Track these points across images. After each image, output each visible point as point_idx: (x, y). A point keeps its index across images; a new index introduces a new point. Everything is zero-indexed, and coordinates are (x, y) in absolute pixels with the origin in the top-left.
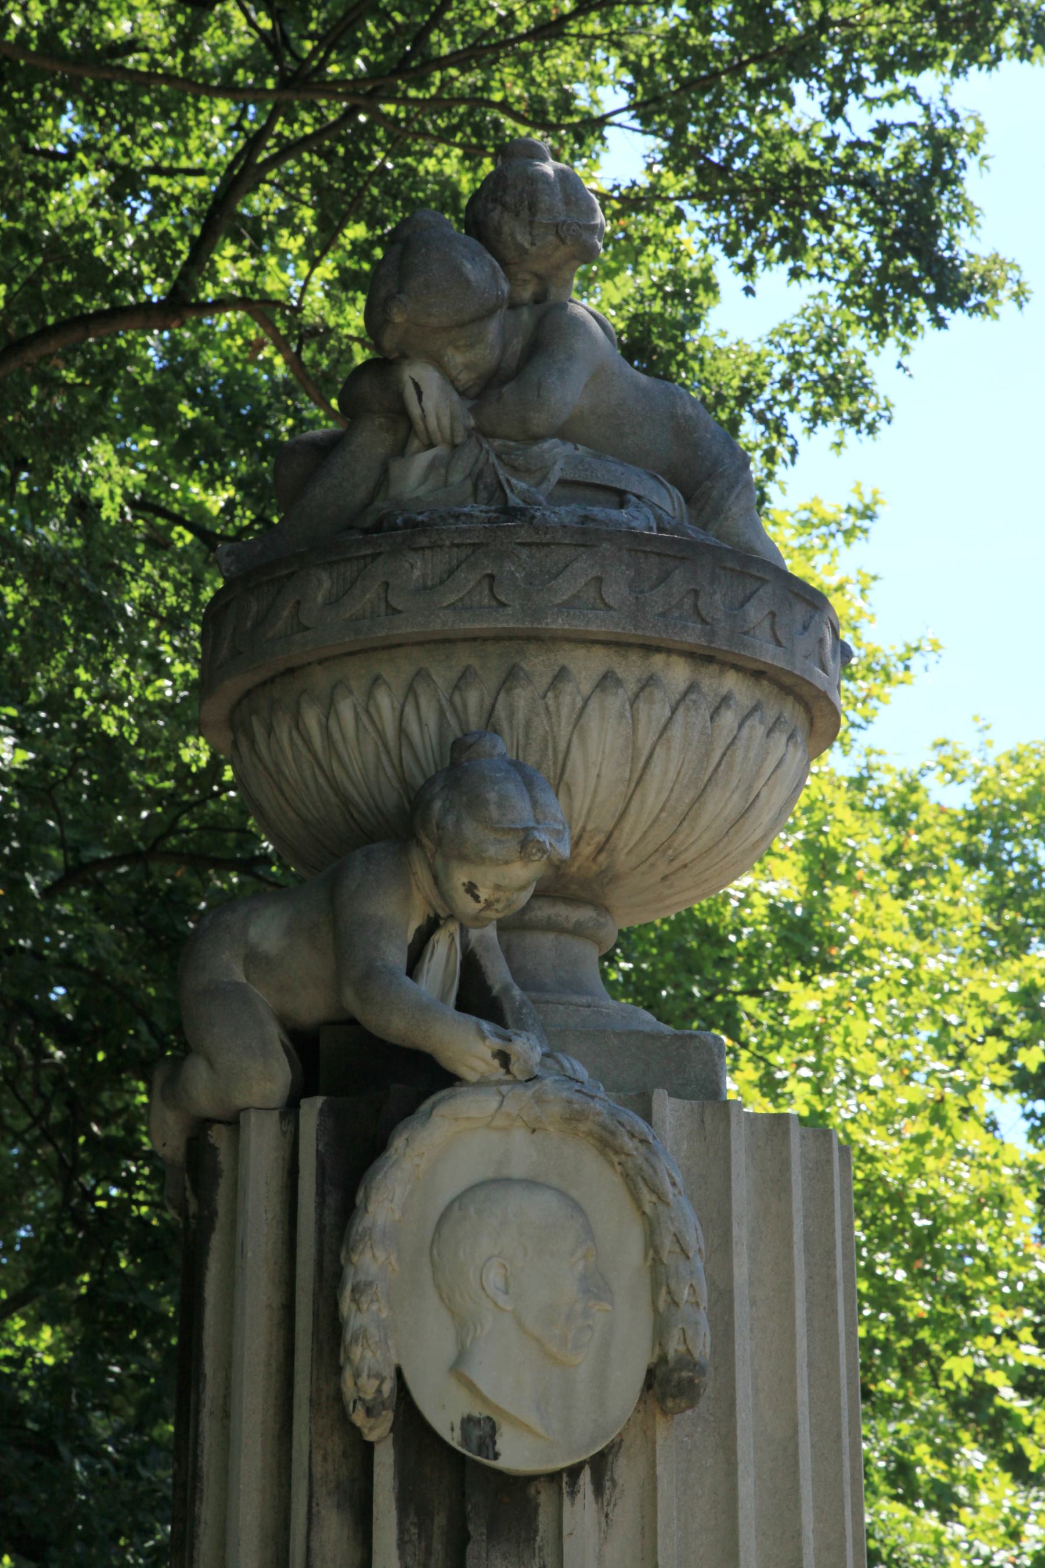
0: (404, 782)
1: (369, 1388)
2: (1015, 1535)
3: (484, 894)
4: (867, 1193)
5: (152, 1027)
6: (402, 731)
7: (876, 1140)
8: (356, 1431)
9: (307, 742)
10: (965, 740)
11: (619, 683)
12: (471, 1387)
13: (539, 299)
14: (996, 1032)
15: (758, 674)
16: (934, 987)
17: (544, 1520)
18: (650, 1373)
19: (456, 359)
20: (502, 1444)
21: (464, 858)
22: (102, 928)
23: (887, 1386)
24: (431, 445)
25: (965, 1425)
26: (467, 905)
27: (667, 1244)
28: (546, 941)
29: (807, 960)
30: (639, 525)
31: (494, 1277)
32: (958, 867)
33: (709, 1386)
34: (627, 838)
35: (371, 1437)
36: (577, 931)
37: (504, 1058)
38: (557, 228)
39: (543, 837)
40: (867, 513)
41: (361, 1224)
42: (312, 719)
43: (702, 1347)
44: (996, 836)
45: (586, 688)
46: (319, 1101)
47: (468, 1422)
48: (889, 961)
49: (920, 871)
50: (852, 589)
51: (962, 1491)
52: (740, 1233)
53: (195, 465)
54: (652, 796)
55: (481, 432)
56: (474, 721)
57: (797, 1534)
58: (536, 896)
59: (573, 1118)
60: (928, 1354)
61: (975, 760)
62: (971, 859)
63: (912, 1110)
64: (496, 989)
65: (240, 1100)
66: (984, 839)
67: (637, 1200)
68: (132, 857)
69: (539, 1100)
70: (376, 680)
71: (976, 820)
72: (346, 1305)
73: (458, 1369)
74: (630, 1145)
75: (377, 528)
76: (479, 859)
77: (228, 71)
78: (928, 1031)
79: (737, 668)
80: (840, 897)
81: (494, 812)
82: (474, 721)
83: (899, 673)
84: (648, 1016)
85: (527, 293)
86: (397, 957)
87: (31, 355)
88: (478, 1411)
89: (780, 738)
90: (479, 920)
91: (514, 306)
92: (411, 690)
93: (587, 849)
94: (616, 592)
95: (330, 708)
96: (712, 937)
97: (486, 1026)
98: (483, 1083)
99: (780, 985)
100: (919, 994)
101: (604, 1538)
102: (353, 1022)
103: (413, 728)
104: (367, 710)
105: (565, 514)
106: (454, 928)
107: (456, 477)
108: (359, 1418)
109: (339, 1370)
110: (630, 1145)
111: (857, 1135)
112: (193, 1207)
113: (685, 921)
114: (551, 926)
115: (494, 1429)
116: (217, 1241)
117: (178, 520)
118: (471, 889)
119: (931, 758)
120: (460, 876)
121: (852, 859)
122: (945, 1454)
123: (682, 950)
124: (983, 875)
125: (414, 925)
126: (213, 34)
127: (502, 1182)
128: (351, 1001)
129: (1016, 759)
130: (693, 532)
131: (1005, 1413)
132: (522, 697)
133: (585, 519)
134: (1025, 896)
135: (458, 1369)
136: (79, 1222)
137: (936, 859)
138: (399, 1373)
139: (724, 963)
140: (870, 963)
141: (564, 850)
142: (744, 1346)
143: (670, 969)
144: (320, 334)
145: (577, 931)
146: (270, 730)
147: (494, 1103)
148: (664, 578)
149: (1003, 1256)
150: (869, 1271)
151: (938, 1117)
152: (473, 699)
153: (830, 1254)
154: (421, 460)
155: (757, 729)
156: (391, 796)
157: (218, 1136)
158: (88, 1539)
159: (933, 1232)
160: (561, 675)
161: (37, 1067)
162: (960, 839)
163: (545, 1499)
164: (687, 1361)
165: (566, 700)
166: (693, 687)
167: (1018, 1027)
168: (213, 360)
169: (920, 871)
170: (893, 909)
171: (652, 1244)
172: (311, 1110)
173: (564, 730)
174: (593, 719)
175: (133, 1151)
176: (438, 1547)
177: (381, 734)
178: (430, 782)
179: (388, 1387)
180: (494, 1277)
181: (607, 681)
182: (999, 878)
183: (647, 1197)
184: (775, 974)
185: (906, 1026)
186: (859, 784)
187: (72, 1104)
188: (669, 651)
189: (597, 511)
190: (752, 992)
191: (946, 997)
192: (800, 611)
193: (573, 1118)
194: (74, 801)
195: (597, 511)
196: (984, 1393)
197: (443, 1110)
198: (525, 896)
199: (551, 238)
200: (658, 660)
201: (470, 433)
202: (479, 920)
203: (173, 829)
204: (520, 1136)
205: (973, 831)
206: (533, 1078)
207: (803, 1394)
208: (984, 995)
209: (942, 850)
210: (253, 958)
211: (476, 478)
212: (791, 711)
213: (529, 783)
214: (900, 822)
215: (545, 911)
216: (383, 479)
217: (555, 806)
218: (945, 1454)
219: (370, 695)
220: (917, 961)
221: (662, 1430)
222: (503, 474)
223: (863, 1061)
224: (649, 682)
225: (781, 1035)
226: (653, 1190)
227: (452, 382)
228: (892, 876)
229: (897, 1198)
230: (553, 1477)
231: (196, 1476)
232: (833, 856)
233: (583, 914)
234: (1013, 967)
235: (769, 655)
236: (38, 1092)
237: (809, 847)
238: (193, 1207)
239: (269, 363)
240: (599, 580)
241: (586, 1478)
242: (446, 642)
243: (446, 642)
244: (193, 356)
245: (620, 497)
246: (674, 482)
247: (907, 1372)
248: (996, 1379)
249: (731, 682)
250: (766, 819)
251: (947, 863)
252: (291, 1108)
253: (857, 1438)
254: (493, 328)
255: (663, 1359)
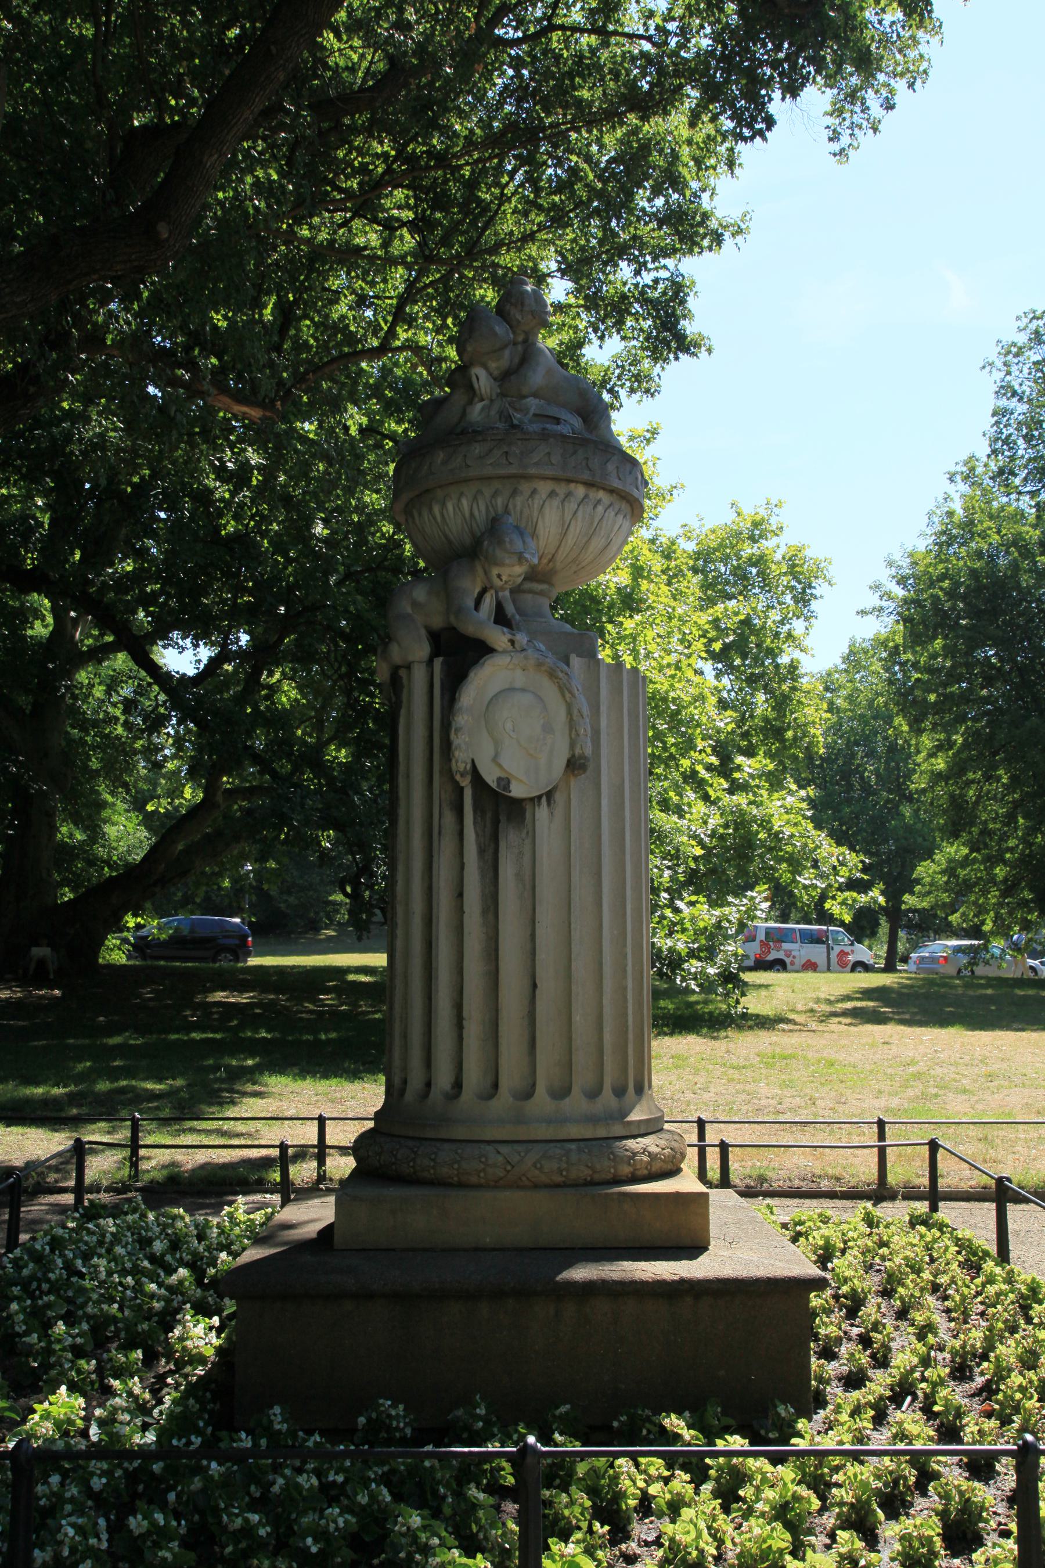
0: (472, 532)
1: (462, 767)
2: (705, 823)
3: (504, 578)
4: (653, 698)
5: (379, 636)
6: (472, 514)
7: (655, 676)
8: (457, 783)
9: (435, 518)
10: (694, 524)
11: (557, 495)
12: (500, 766)
13: (525, 341)
14: (704, 636)
15: (612, 491)
16: (680, 619)
17: (528, 815)
18: (569, 761)
19: (493, 365)
20: (512, 787)
21: (496, 564)
22: (359, 597)
23: (658, 771)
24: (482, 400)
25: (688, 784)
26: (498, 583)
27: (575, 712)
28: (529, 596)
29: (632, 609)
30: (565, 432)
31: (509, 726)
32: (690, 574)
33: (591, 766)
34: (561, 556)
35: (463, 784)
36: (541, 593)
37: (512, 642)
38: (532, 312)
39: (527, 556)
40: (654, 432)
41: (458, 705)
42: (436, 509)
43: (588, 751)
44: (705, 561)
45: (544, 497)
46: (441, 659)
47: (499, 779)
48: (661, 607)
49: (675, 576)
50: (650, 464)
51: (686, 808)
52: (603, 709)
53: (392, 415)
54: (570, 540)
55: (503, 395)
56: (500, 510)
57: (623, 820)
58: (525, 579)
59: (539, 665)
60: (675, 759)
61: (698, 531)
62: (695, 570)
63: (669, 665)
64: (509, 616)
65: (411, 658)
66: (701, 562)
67: (563, 696)
68: (369, 569)
69: (526, 658)
70: (462, 494)
71: (698, 555)
72: (452, 736)
73: (495, 759)
74: (561, 675)
75: (462, 433)
76: (501, 564)
77: (403, 257)
78: (677, 636)
79: (604, 489)
80: (644, 585)
81: (508, 546)
82: (500, 510)
83: (668, 497)
84: (568, 626)
85: (520, 339)
86: (470, 603)
87: (327, 370)
88: (503, 775)
89: (620, 517)
90: (502, 589)
91: (515, 344)
92: (475, 498)
93: (545, 561)
94: (556, 459)
95: (443, 505)
96: (595, 600)
97: (505, 630)
98: (504, 652)
99: (621, 619)
100: (675, 622)
101: (551, 821)
102: (454, 629)
103: (476, 513)
104: (458, 506)
105: (534, 427)
106: (493, 592)
107: (493, 413)
108: (458, 778)
109: (450, 760)
110: (561, 675)
111: (648, 674)
112: (394, 699)
113: (584, 594)
114: (530, 591)
115: (509, 782)
116: (403, 712)
117: (386, 437)
118: (499, 576)
119: (681, 531)
120: (495, 571)
121: (650, 571)
122: (680, 795)
123: (584, 606)
124: (700, 576)
125: (477, 590)
126: (397, 242)
127: (512, 689)
128: (452, 619)
129: (713, 531)
130: (587, 435)
131: (703, 780)
132: (519, 500)
133: (544, 429)
134: (716, 585)
135: (495, 759)
136: (354, 710)
137: (681, 571)
138: (473, 761)
139: (599, 611)
140: (653, 608)
141: (536, 561)
142: (604, 751)
143: (579, 613)
144: (440, 360)
145: (541, 593)
146: (420, 514)
147: (508, 659)
148: (575, 453)
149: (704, 719)
150: (654, 727)
151: (678, 668)
152: (500, 501)
153: (638, 716)
154: (479, 406)
155: (611, 513)
156: (468, 540)
157: (403, 673)
158: (361, 824)
159: (678, 712)
160: (534, 492)
161: (336, 651)
162: (691, 563)
163: (528, 808)
164: (583, 757)
165: (536, 501)
166: (586, 496)
167: (712, 634)
168: (398, 372)
169: (675, 576)
170: (664, 588)
171: (569, 713)
172: (438, 662)
173: (535, 514)
174: (547, 509)
175: (372, 682)
176: (488, 824)
177: (464, 516)
178: (483, 534)
179: (469, 766)
180: (509, 726)
181: (552, 494)
182: (706, 577)
183: (568, 695)
184: (619, 615)
185: (669, 634)
186: (652, 541)
187: (349, 664)
188: (577, 482)
189: (548, 426)
190: (611, 622)
191: (685, 622)
192: (628, 466)
193: (539, 665)
194: (347, 548)
195: (548, 426)
196: (694, 773)
197: (488, 662)
198: (520, 580)
199: (530, 317)
200: (572, 486)
201: (498, 395)
202: (502, 589)
203: (385, 559)
204: (519, 672)
205: (697, 559)
206: (523, 650)
207: (626, 750)
208: (700, 622)
209: (684, 567)
210: (415, 604)
211: (501, 413)
212: (624, 506)
213: (521, 534)
214: (668, 557)
215: (528, 585)
216: (464, 414)
217: (532, 544)
218: (680, 795)
219: (459, 500)
220: (674, 609)
221: (573, 782)
222: (511, 411)
223: (652, 647)
224: (569, 494)
225: (621, 638)
226: (570, 692)
227: (491, 374)
228: (664, 577)
229: (665, 700)
230: (532, 799)
231: (397, 798)
232: (642, 568)
233: (544, 587)
234: (711, 611)
235: (616, 484)
236: (336, 659)
237: (633, 566)
238: (394, 699)
239: (421, 373)
240: (549, 454)
241: (544, 799)
242: (489, 478)
243: (489, 478)
244: (391, 371)
245: (557, 421)
246: (580, 415)
247: (667, 766)
248: (699, 768)
249: (601, 494)
250: (615, 549)
251: (686, 572)
252: (430, 662)
253: (646, 789)
254: (507, 353)
255: (573, 756)
